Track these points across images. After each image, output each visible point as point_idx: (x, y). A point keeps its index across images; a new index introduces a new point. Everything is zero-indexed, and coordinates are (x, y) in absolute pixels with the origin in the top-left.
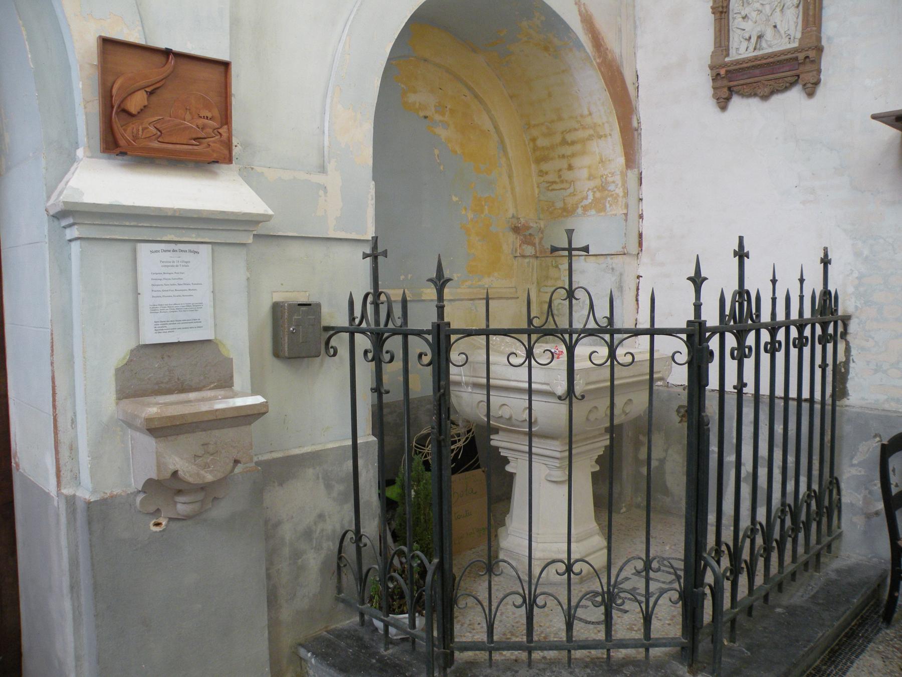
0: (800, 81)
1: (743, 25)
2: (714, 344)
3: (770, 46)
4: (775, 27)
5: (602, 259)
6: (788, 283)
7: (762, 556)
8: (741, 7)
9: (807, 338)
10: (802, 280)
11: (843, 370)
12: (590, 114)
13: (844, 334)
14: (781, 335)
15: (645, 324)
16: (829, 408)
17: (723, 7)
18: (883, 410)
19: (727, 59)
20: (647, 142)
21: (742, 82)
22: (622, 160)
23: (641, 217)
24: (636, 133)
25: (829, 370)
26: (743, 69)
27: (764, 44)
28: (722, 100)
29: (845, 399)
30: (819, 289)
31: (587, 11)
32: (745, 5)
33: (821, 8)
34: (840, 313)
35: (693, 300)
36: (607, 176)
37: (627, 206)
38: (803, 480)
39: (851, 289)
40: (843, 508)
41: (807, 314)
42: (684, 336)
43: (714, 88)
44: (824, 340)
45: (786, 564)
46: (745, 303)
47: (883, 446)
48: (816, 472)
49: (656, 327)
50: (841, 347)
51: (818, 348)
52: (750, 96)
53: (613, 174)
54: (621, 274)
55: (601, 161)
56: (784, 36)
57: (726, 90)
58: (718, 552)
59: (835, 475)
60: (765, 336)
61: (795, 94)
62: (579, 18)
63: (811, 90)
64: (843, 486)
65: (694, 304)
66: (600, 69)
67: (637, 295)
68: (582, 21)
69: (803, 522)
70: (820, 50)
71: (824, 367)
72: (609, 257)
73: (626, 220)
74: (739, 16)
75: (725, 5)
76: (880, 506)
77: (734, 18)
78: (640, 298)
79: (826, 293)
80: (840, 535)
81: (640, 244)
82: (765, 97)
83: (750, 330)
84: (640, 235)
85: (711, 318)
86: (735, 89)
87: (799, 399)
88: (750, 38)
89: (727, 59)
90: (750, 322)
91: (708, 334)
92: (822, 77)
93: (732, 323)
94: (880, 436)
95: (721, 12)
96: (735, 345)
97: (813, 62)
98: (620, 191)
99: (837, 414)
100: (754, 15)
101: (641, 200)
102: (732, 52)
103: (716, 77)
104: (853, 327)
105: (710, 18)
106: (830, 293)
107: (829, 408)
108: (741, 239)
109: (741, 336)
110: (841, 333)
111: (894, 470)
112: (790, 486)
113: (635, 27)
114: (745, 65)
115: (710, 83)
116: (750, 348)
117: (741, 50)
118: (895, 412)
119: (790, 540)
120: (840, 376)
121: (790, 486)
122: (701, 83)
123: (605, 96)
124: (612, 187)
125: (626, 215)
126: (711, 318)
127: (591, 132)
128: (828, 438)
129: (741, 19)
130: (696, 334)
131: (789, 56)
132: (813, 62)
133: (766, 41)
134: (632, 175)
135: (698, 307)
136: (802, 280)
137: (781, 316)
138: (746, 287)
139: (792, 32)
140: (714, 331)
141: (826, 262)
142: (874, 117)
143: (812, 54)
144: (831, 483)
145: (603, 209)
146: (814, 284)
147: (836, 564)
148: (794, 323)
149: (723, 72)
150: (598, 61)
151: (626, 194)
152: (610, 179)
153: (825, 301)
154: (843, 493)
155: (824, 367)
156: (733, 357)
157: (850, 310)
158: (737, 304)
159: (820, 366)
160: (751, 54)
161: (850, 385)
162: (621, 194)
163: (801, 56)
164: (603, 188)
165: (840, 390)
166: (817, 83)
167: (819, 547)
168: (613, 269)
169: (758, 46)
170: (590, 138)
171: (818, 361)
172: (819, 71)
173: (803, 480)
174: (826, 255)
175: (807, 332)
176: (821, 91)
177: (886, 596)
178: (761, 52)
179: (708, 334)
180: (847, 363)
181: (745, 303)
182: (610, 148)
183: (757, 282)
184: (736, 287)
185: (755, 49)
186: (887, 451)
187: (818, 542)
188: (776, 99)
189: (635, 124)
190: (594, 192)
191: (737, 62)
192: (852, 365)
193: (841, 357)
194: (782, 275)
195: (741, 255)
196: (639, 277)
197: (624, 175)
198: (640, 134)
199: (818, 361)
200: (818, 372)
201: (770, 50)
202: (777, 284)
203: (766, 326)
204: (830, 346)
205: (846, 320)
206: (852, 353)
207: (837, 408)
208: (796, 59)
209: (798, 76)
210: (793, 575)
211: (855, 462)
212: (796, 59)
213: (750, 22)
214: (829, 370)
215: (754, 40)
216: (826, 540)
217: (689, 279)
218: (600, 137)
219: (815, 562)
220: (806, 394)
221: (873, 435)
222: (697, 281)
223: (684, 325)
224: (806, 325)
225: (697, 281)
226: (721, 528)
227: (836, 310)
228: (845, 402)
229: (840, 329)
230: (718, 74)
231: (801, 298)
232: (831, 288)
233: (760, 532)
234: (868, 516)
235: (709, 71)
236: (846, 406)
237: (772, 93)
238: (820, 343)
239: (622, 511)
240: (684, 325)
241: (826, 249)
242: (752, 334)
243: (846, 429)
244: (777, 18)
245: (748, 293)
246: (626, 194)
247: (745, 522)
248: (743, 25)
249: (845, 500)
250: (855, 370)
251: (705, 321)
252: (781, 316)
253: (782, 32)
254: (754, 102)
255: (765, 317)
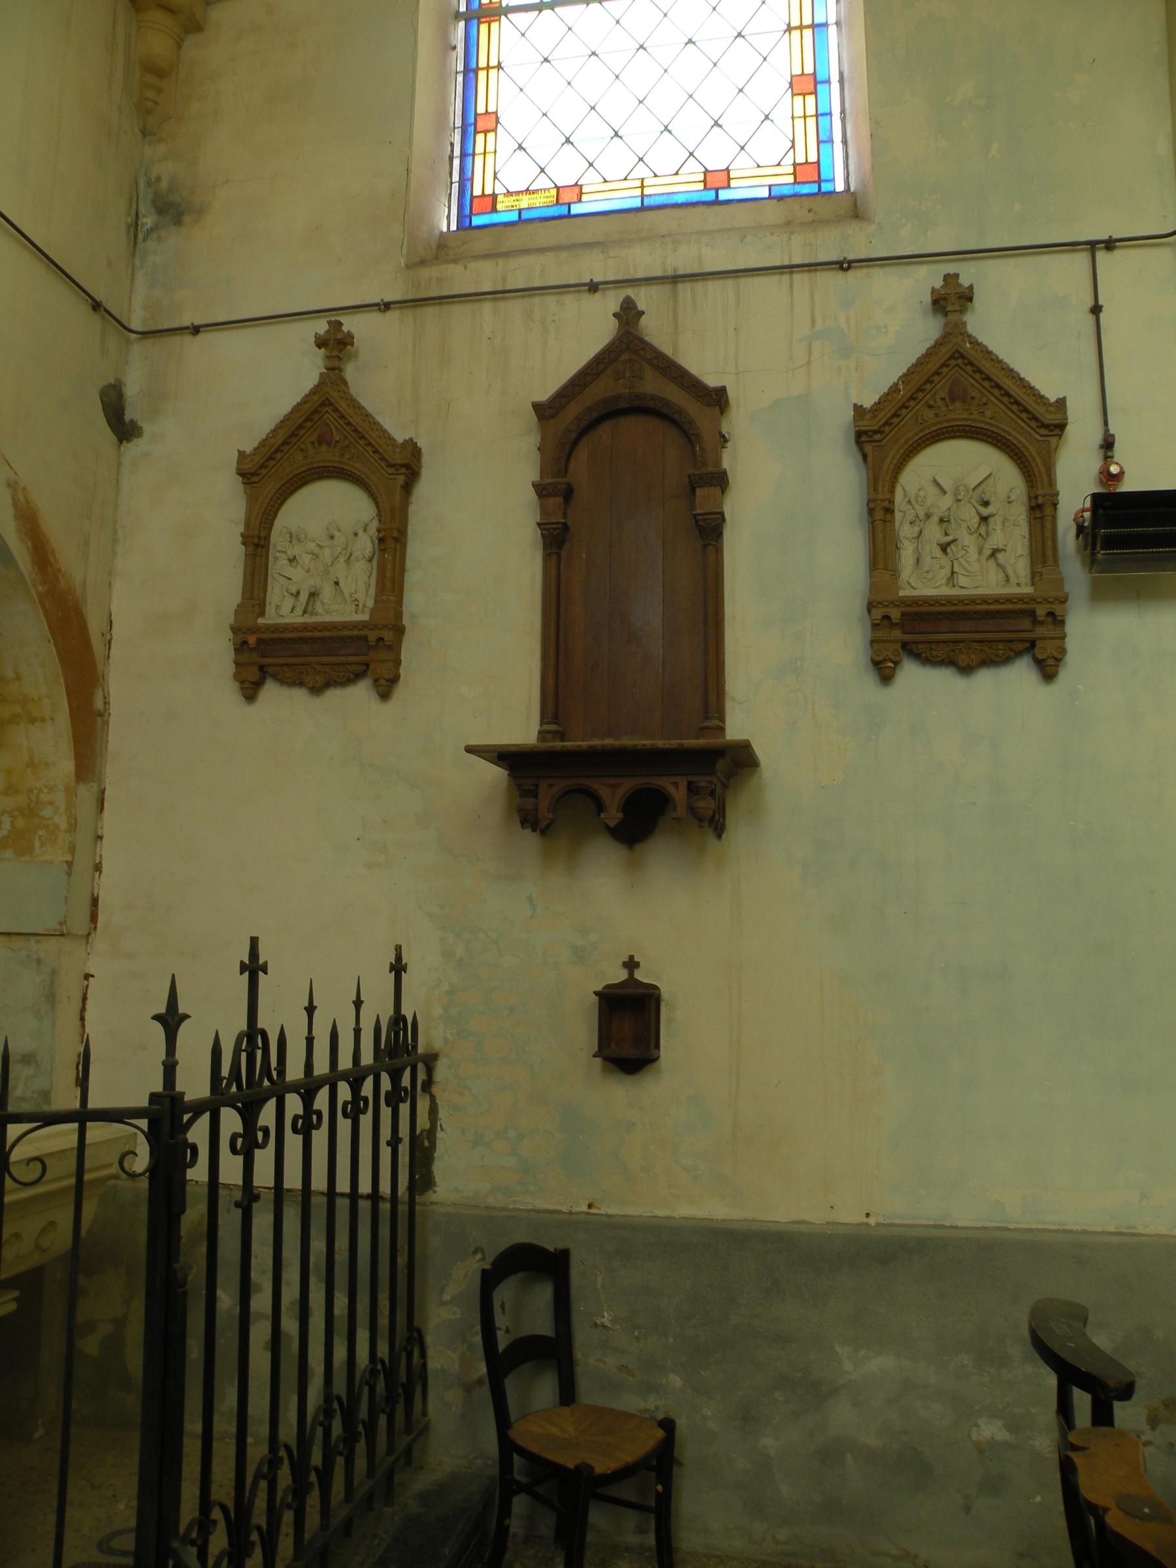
0: (369, 673)
1: (289, 571)
2: (198, 1134)
3: (327, 612)
4: (337, 583)
5: (18, 943)
6: (335, 1010)
7: (289, 1507)
8: (287, 544)
9: (366, 1100)
10: (358, 1003)
11: (426, 1144)
12: (18, 678)
13: (428, 1085)
14: (321, 1101)
15: (67, 1100)
16: (403, 1209)
17: (259, 537)
18: (486, 1207)
19: (260, 621)
20: (121, 738)
21: (282, 661)
22: (67, 766)
23: (98, 868)
24: (99, 720)
25: (404, 1149)
26: (284, 640)
27: (319, 608)
28: (248, 685)
29: (430, 1192)
30: (387, 1013)
31: (27, 501)
32: (294, 541)
33: (403, 570)
34: (421, 1050)
35: (162, 1056)
36: (40, 791)
37: (72, 849)
38: (363, 1335)
39: (437, 1010)
40: (430, 1378)
41: (367, 1058)
42: (143, 1123)
43: (237, 664)
44: (393, 1100)
45: (334, 1503)
46: (259, 1053)
47: (484, 1272)
48: (384, 1321)
49: (90, 1106)
50: (423, 1105)
51: (386, 1112)
52: (291, 684)
53: (51, 789)
54: (54, 973)
55: (32, 764)
56: (349, 600)
57: (255, 669)
58: (204, 1525)
59: (416, 1324)
60: (294, 1106)
61: (361, 692)
62: (10, 511)
63: (386, 688)
64: (429, 1340)
65: (164, 1063)
66: (42, 603)
67: (83, 1009)
68: (16, 517)
69: (363, 1422)
70: (400, 631)
71: (394, 1143)
72: (33, 940)
73: (69, 874)
74: (283, 556)
75: (263, 534)
76: (482, 1369)
77: (276, 558)
78: (88, 1016)
79: (398, 1019)
80: (426, 1427)
81: (94, 918)
82: (317, 690)
83: (265, 1100)
84: (95, 901)
85: (194, 1084)
86: (270, 670)
87: (354, 1195)
88: (298, 593)
89: (260, 621)
90: (266, 1083)
91: (186, 1117)
92: (401, 671)
93: (234, 1089)
94: (482, 1251)
95: (257, 545)
96: (240, 1129)
97: (389, 647)
98: (62, 821)
99: (418, 1219)
100: (306, 558)
101: (100, 838)
102: (270, 610)
103: (241, 647)
104: (442, 1071)
105: (239, 551)
106: (404, 1019)
107: (403, 1209)
108: (254, 942)
109: (249, 1114)
110: (424, 1083)
111: (503, 1306)
112: (340, 1353)
113: (115, 541)
114: (287, 635)
115: (230, 655)
116: (266, 1131)
117: (282, 610)
118: (503, 1209)
119: (340, 1461)
120: (422, 1153)
121: (340, 1353)
122: (219, 652)
123: (49, 651)
124: (47, 812)
125: (70, 864)
126: (194, 1084)
127: (17, 709)
128: (402, 1260)
129: (286, 562)
130: (166, 1116)
131: (355, 632)
132: (389, 647)
133: (322, 603)
134: (86, 793)
135: (170, 1069)
136: (358, 1003)
137: (321, 1067)
138: (261, 1025)
139: (361, 596)
140: (198, 1109)
141: (398, 968)
142: (470, 750)
143: (388, 636)
144: (409, 1340)
145: (28, 850)
146: (378, 1007)
147: (421, 1483)
148: (344, 1076)
149: (252, 640)
150: (40, 589)
151: (73, 827)
152: (45, 797)
153: (397, 1035)
154: (431, 1352)
155: (394, 1143)
156: (234, 1151)
157: (438, 1044)
158: (244, 1055)
159: (388, 1144)
160: (297, 619)
161: (439, 1168)
162: (64, 826)
163: (372, 636)
164: (30, 812)
165: (422, 1179)
166: (394, 680)
167: (391, 1459)
168: (39, 961)
169: (310, 609)
170: (14, 719)
171: (386, 1133)
172: (398, 662)
173: (363, 1335)
174: (399, 957)
175: (367, 1089)
176: (399, 692)
177: (493, 1523)
178: (314, 619)
179: (186, 1117)
180: (431, 1133)
181: (259, 1053)
182: (52, 742)
183: (280, 1013)
184: (243, 1026)
185: (305, 612)
186: (489, 1280)
187: (391, 1449)
188: (334, 695)
189: (99, 704)
190: (14, 818)
191: (277, 628)
192: (440, 1134)
193: (423, 1122)
194: (322, 997)
195: (253, 968)
196: (87, 976)
197: (70, 793)
198: (107, 723)
199: (386, 1133)
200: (386, 1153)
201: (327, 619)
202: (316, 1014)
203: (294, 1088)
204: (405, 1108)
205: (430, 1060)
206: (440, 1115)
207: (417, 1208)
208: (365, 638)
209: (367, 665)
210: (348, 1525)
211: (446, 1297)
212: (365, 638)
213: (299, 569)
214: (404, 1149)
215: (304, 597)
216: (402, 1442)
217: (156, 1018)
218: (33, 720)
219: (387, 1487)
220: (365, 1187)
221: (472, 1249)
222: (171, 1020)
223: (144, 1102)
224: (364, 1078)
225: (171, 1020)
226: (210, 1473)
227: (415, 1047)
228: (431, 1196)
229: (421, 1076)
230: (245, 643)
231: (357, 1032)
232: (407, 1011)
233: (286, 1463)
234: (468, 1388)
235: (231, 635)
236: (432, 1203)
237: (328, 684)
238: (388, 1105)
239: (37, 1435)
240: (144, 1102)
241: (398, 949)
242: (271, 1104)
243: (432, 1243)
244: (340, 571)
245: (264, 1034)
246: (73, 827)
247: (257, 1451)
248: (289, 571)
249: (433, 1364)
250: (445, 1141)
251: (182, 1094)
252: (321, 1067)
253: (347, 594)
254: (299, 695)
255: (295, 1071)
